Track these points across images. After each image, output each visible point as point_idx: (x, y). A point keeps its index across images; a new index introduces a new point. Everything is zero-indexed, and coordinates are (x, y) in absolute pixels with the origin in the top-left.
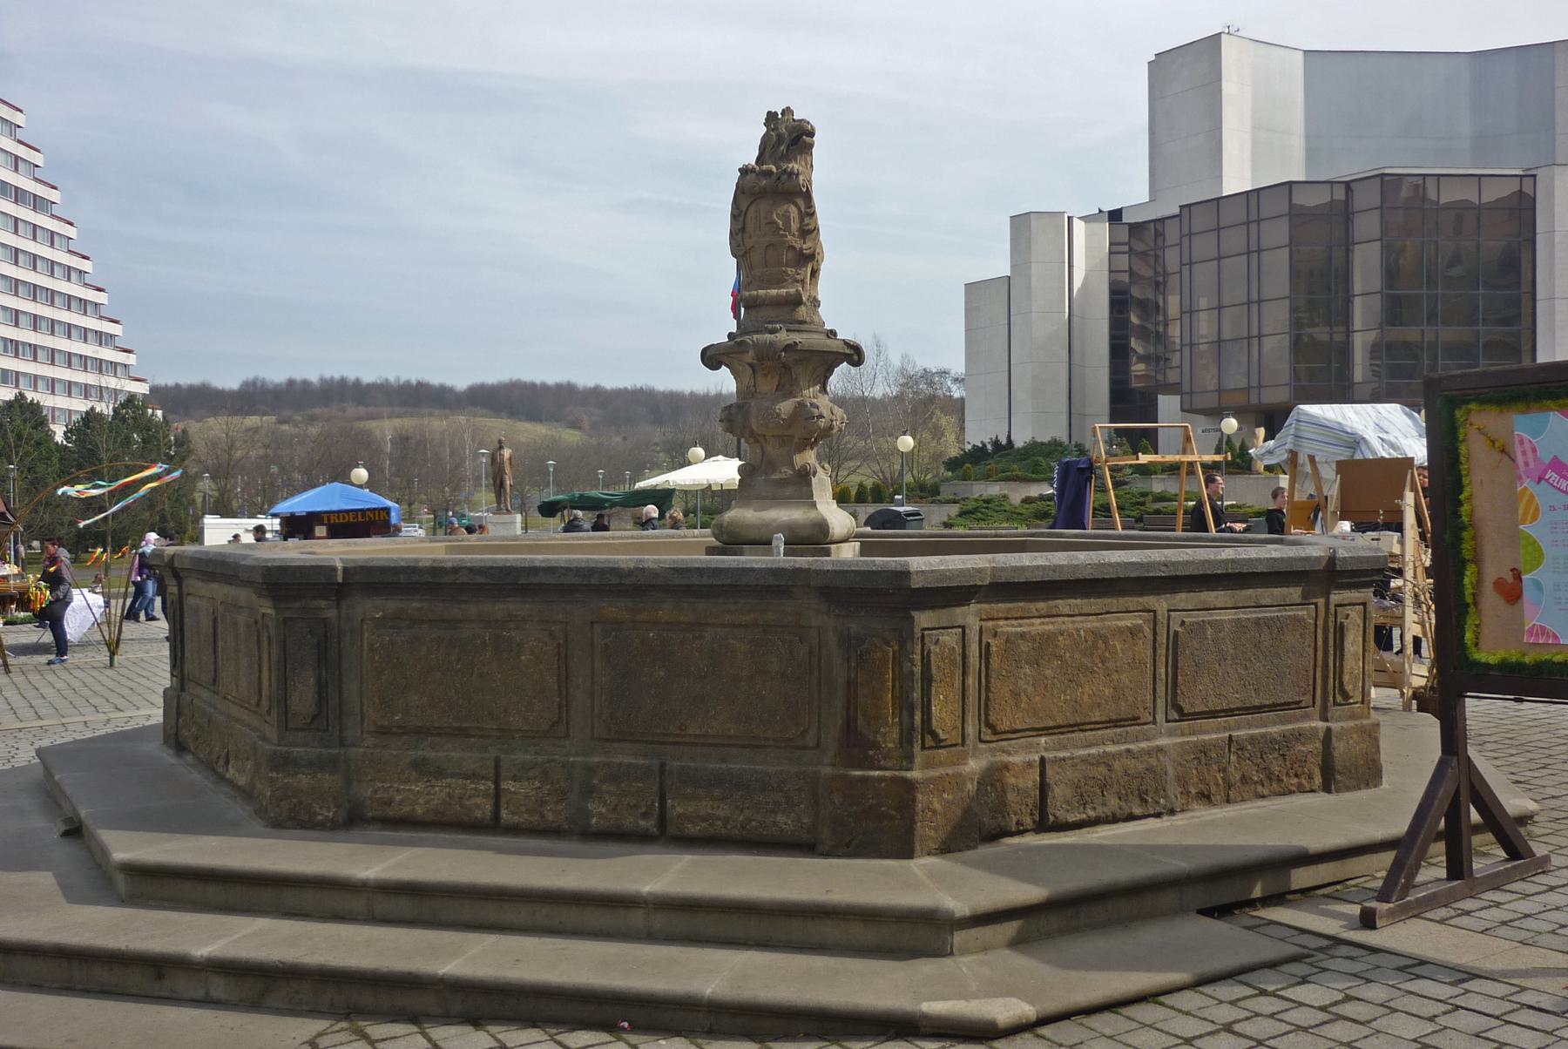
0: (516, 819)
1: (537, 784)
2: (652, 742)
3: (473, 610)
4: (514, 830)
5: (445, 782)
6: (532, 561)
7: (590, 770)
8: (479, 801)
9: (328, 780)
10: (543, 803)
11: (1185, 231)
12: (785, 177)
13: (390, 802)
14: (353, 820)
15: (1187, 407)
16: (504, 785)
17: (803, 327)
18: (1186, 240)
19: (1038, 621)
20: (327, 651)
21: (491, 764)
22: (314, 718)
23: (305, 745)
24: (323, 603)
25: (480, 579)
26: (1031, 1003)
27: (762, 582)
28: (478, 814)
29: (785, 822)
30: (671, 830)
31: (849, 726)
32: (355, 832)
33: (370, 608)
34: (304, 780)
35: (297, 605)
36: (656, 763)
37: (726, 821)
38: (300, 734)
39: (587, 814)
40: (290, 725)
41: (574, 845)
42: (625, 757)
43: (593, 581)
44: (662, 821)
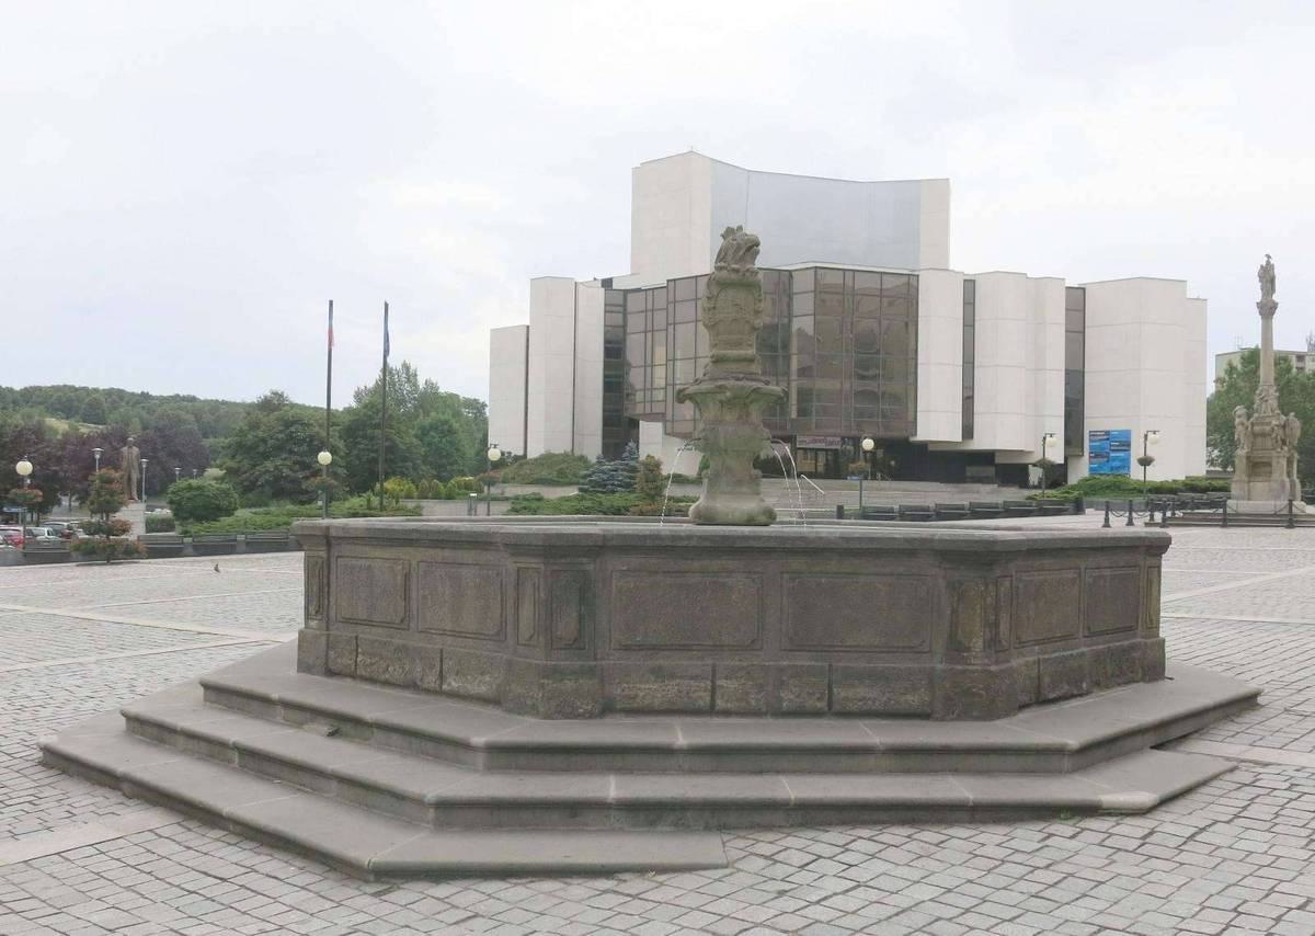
0: (729, 705)
1: (743, 681)
2: (822, 651)
3: (696, 565)
4: (726, 713)
5: (674, 683)
6: (742, 532)
7: (781, 670)
8: (702, 694)
9: (587, 684)
10: (747, 693)
11: (671, 299)
12: (748, 274)
13: (636, 696)
14: (607, 709)
15: (669, 431)
16: (719, 683)
17: (753, 376)
18: (671, 307)
19: (1036, 573)
20: (585, 593)
21: (710, 668)
22: (575, 640)
23: (566, 660)
24: (585, 560)
25: (707, 544)
26: (1154, 792)
27: (901, 547)
28: (701, 703)
29: (913, 700)
30: (837, 707)
31: (952, 637)
32: (608, 720)
33: (616, 564)
34: (569, 684)
35: (563, 561)
36: (826, 664)
37: (874, 700)
38: (563, 652)
39: (780, 700)
40: (554, 647)
41: (770, 720)
42: (803, 660)
43: (787, 546)
44: (830, 704)
